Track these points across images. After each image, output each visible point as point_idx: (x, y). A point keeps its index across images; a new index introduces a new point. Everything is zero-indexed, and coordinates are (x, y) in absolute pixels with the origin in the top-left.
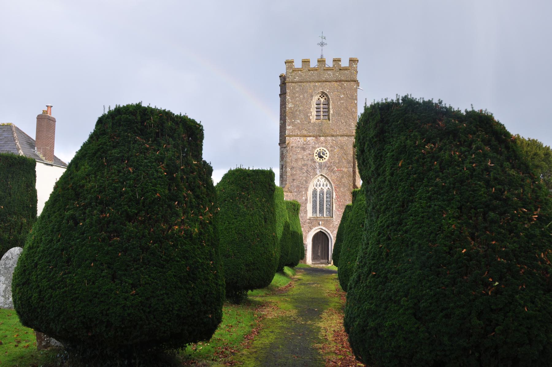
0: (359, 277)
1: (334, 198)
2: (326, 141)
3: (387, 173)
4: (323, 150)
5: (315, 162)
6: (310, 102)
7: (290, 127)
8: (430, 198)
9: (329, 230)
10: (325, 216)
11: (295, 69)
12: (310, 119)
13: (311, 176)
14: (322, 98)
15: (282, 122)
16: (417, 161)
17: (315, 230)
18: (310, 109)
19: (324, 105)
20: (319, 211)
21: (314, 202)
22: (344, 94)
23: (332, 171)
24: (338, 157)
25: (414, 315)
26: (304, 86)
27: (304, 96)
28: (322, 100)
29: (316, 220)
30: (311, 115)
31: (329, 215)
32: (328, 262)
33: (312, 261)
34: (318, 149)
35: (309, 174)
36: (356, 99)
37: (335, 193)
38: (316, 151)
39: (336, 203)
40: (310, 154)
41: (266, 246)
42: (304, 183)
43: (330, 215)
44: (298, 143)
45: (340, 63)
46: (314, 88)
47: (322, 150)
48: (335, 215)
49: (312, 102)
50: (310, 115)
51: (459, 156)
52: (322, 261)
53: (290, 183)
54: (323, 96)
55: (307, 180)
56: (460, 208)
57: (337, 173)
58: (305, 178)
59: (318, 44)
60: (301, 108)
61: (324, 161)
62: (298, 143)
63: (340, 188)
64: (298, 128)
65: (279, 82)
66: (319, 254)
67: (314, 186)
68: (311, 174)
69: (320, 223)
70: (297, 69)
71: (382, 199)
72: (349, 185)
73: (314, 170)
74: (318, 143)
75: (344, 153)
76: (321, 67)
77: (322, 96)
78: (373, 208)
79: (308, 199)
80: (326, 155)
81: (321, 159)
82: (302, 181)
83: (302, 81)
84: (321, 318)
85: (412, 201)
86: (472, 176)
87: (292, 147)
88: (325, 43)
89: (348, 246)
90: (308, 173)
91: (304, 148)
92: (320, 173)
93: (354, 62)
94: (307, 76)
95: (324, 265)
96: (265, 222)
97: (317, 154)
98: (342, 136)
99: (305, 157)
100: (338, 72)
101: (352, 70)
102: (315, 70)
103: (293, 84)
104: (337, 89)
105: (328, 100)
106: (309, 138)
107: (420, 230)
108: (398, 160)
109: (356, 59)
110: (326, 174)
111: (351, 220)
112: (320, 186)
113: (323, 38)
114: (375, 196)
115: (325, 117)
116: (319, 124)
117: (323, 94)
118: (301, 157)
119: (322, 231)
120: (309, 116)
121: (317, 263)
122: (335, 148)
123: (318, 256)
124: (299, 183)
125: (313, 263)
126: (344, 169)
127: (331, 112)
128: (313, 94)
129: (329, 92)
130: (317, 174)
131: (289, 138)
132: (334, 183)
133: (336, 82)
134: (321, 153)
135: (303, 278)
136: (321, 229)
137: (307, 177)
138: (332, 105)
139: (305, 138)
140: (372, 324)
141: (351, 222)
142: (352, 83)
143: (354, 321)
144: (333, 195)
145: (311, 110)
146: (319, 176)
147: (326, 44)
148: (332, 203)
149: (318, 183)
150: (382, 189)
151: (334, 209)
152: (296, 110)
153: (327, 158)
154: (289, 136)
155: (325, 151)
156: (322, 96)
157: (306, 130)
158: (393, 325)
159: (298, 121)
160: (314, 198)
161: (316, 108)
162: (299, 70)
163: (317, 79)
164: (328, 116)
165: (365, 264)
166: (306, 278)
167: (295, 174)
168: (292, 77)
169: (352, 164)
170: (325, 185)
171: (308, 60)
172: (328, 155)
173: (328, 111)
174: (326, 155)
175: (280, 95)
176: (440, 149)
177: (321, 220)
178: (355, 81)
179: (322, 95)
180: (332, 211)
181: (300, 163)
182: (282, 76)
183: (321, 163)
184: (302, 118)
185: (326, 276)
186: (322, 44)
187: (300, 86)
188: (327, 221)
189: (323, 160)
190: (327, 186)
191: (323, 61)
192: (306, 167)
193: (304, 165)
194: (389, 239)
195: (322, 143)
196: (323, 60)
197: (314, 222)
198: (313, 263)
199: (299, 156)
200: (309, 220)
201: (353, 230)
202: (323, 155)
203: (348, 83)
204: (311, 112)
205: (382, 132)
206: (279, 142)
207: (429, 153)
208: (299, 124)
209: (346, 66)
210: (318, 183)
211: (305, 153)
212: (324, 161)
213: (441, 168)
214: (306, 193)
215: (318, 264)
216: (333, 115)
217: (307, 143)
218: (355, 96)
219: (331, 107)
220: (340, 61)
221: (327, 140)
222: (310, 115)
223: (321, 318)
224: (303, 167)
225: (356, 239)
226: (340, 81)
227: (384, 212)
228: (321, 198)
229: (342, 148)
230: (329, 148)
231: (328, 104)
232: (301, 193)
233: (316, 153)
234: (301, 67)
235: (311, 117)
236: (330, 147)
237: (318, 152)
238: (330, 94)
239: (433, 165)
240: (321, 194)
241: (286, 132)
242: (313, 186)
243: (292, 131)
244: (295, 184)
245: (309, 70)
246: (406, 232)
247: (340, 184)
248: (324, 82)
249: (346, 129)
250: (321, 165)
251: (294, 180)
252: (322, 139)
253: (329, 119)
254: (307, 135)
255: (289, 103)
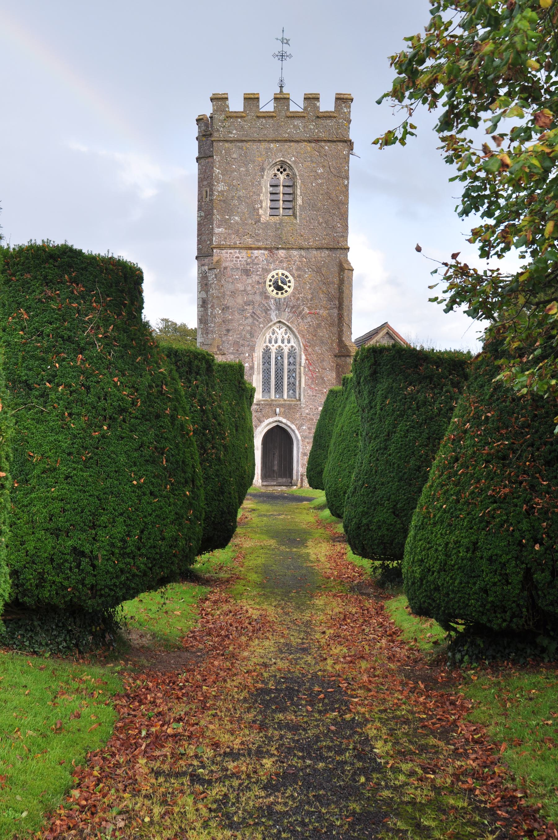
0: (355, 488)
1: (303, 365)
2: (288, 258)
3: (378, 407)
4: (283, 274)
5: (267, 297)
6: (259, 182)
7: (220, 230)
8: (407, 430)
9: (293, 423)
10: (285, 397)
11: (230, 115)
12: (258, 214)
13: (260, 323)
14: (281, 173)
15: (203, 214)
16: (401, 400)
17: (268, 425)
18: (259, 195)
19: (286, 188)
20: (276, 388)
21: (266, 373)
22: (324, 167)
23: (299, 314)
24: (310, 288)
25: (394, 513)
26: (247, 148)
27: (247, 170)
28: (282, 177)
29: (270, 405)
30: (261, 207)
31: (292, 395)
32: (291, 483)
33: (262, 482)
34: (274, 273)
35: (258, 321)
36: (347, 178)
37: (306, 355)
38: (269, 277)
39: (306, 375)
40: (258, 283)
41: (238, 460)
42: (248, 336)
43: (295, 395)
44: (236, 261)
45: (318, 104)
46: (267, 153)
47: (280, 275)
48: (304, 396)
49: (263, 182)
50: (259, 206)
51: (432, 398)
52: (280, 480)
53: (221, 337)
54: (285, 170)
55: (253, 331)
56: (428, 438)
57: (309, 319)
58: (249, 328)
59: (275, 56)
60: (241, 193)
61: (285, 295)
62: (236, 261)
63: (314, 346)
64: (237, 232)
65: (195, 131)
66: (276, 468)
67: (265, 342)
68: (260, 320)
69: (278, 410)
70: (235, 115)
71: (373, 429)
72: (329, 341)
73: (266, 313)
74: (274, 262)
75: (321, 281)
76: (280, 111)
77: (281, 170)
78: (367, 435)
79: (256, 367)
80: (288, 284)
81: (280, 292)
82: (244, 333)
83: (244, 139)
84: (307, 546)
85: (395, 432)
86: (439, 414)
87: (225, 268)
88: (288, 54)
89: (338, 459)
90: (254, 319)
91: (247, 270)
92: (277, 318)
93: (344, 102)
94: (254, 129)
95: (284, 488)
96: (237, 430)
97: (271, 283)
98: (317, 249)
99: (249, 288)
100: (313, 121)
101: (340, 119)
102: (268, 116)
103: (227, 145)
104: (311, 157)
105: (291, 177)
106: (256, 251)
107: (399, 454)
108: (386, 398)
109: (349, 97)
110: (288, 321)
111: (342, 427)
112: (276, 342)
113: (285, 41)
114: (368, 424)
115: (287, 210)
116: (275, 223)
117: (283, 166)
118: (242, 289)
119: (281, 425)
120: (258, 209)
121: (272, 483)
122: (305, 271)
123: (274, 471)
124: (239, 336)
125: (265, 483)
126: (321, 312)
127: (299, 201)
128: (265, 166)
129: (295, 162)
130: (271, 321)
131: (218, 251)
132: (303, 337)
133: (310, 142)
134: (280, 281)
135: (259, 508)
136: (279, 421)
137: (252, 325)
138: (301, 187)
139: (249, 251)
140: (364, 521)
141: (342, 429)
142: (340, 145)
143: (352, 521)
144: (301, 359)
145: (262, 198)
146: (275, 324)
147: (290, 56)
148: (300, 374)
149: (274, 337)
150: (373, 419)
151: (303, 385)
152: (233, 197)
153: (289, 290)
154: (220, 247)
155: (287, 277)
156: (281, 170)
157: (251, 237)
158: (379, 521)
159: (237, 218)
160: (266, 364)
161: (271, 194)
162: (238, 115)
163: (271, 136)
164: (293, 208)
165: (360, 478)
166: (264, 508)
167: (232, 320)
168: (225, 130)
169: (337, 303)
170: (286, 341)
171: (256, 96)
172: (292, 284)
173: (294, 199)
174: (288, 284)
175: (198, 159)
176: (418, 392)
177: (279, 406)
178: (345, 141)
179: (281, 167)
180: (300, 388)
181: (240, 300)
182: (202, 119)
183: (279, 299)
184: (244, 213)
185: (294, 504)
186: (282, 56)
187: (241, 148)
188: (290, 407)
189: (282, 294)
190: (289, 342)
191: (285, 98)
192: (251, 307)
193: (248, 303)
194: (378, 460)
195: (281, 262)
196: (285, 96)
197: (267, 410)
198: (265, 483)
199: (239, 285)
200: (257, 405)
201: (344, 439)
202: (282, 285)
203: (333, 145)
204: (261, 202)
205: (375, 372)
206: (196, 254)
207: (410, 394)
208: (237, 223)
209: (329, 110)
210: (274, 337)
211: (250, 281)
212: (285, 295)
213: (417, 407)
214: (251, 356)
215: (274, 486)
216: (302, 208)
217: (253, 260)
218: (345, 171)
219: (298, 192)
220: (318, 99)
221: (290, 256)
222: (259, 206)
223: (307, 546)
224: (246, 307)
225: (349, 451)
226: (317, 141)
227: (375, 439)
228: (279, 365)
229: (318, 271)
230: (294, 271)
231: (293, 186)
232: (242, 355)
233: (270, 280)
234: (242, 110)
235: (261, 212)
236: (296, 270)
237: (273, 279)
238: (296, 167)
239: (412, 404)
240: (279, 358)
241: (214, 239)
242: (263, 342)
243: (226, 238)
244: (231, 338)
245: (258, 117)
246: (390, 455)
247: (315, 338)
248: (286, 141)
249: (327, 235)
250: (278, 303)
251: (228, 331)
252: (282, 253)
253: (294, 215)
254: (253, 246)
255: (218, 183)
